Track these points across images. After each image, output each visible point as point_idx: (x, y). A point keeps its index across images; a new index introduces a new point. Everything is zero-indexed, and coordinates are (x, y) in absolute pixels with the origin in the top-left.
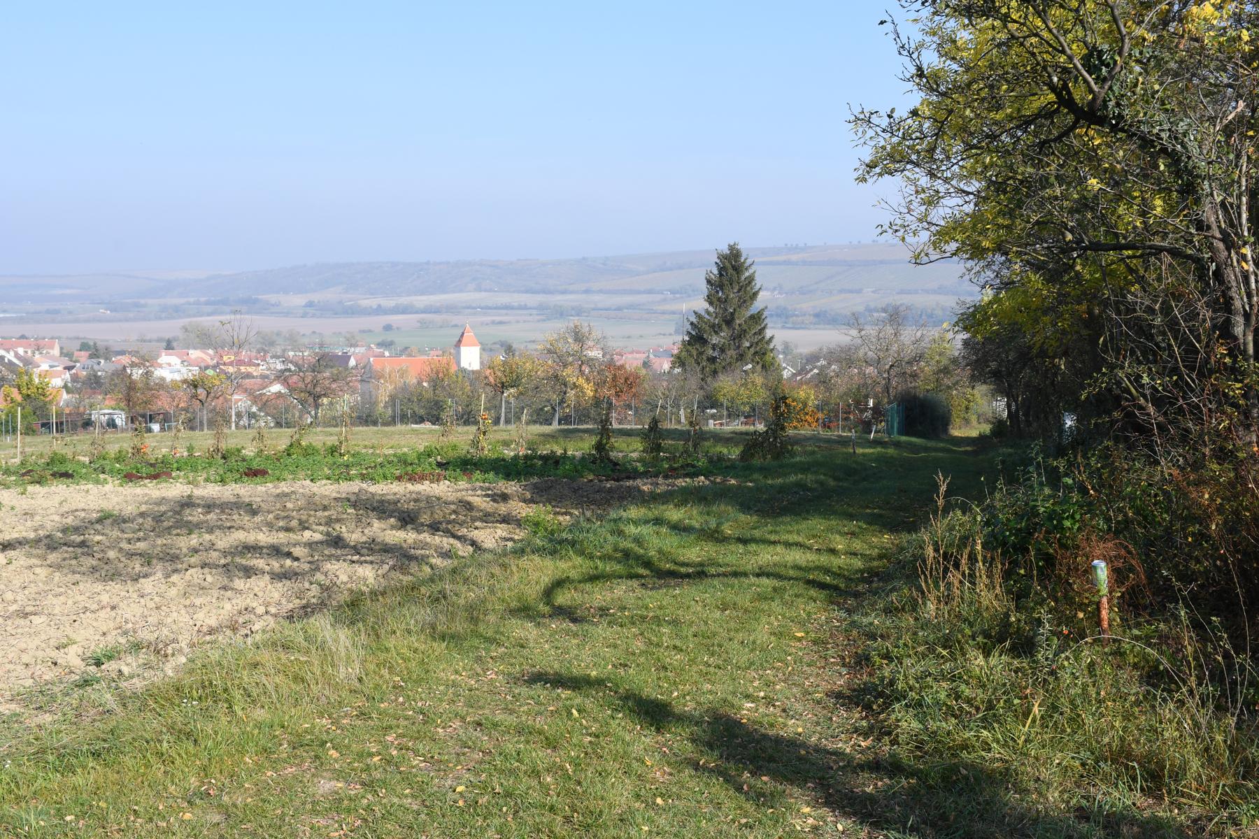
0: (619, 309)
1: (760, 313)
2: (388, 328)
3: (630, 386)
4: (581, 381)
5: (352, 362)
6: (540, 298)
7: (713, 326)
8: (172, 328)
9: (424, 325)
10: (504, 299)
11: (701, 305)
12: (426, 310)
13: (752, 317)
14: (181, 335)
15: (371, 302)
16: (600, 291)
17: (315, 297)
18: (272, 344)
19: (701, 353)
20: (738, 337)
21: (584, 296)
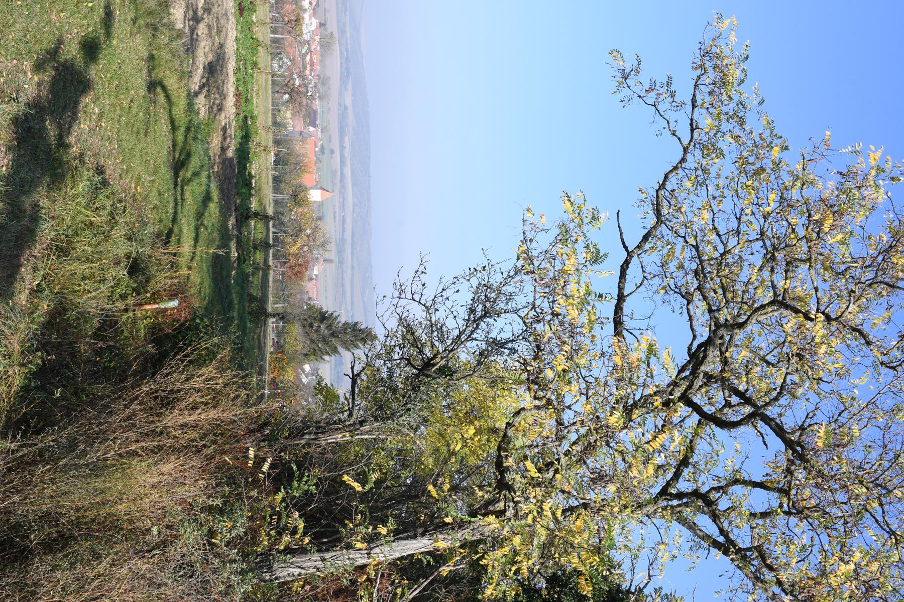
0: (343, 285)
1: (338, 352)
2: (332, 152)
3: (296, 274)
4: (298, 245)
5: (311, 129)
6: (349, 240)
7: (330, 326)
8: (332, 27)
9: (334, 173)
10: (349, 220)
11: (343, 320)
12: (342, 173)
13: (336, 348)
14: (329, 31)
15: (347, 144)
16: (353, 275)
17: (350, 112)
18: (323, 84)
19: (315, 319)
20: (325, 340)
21: (350, 265)
